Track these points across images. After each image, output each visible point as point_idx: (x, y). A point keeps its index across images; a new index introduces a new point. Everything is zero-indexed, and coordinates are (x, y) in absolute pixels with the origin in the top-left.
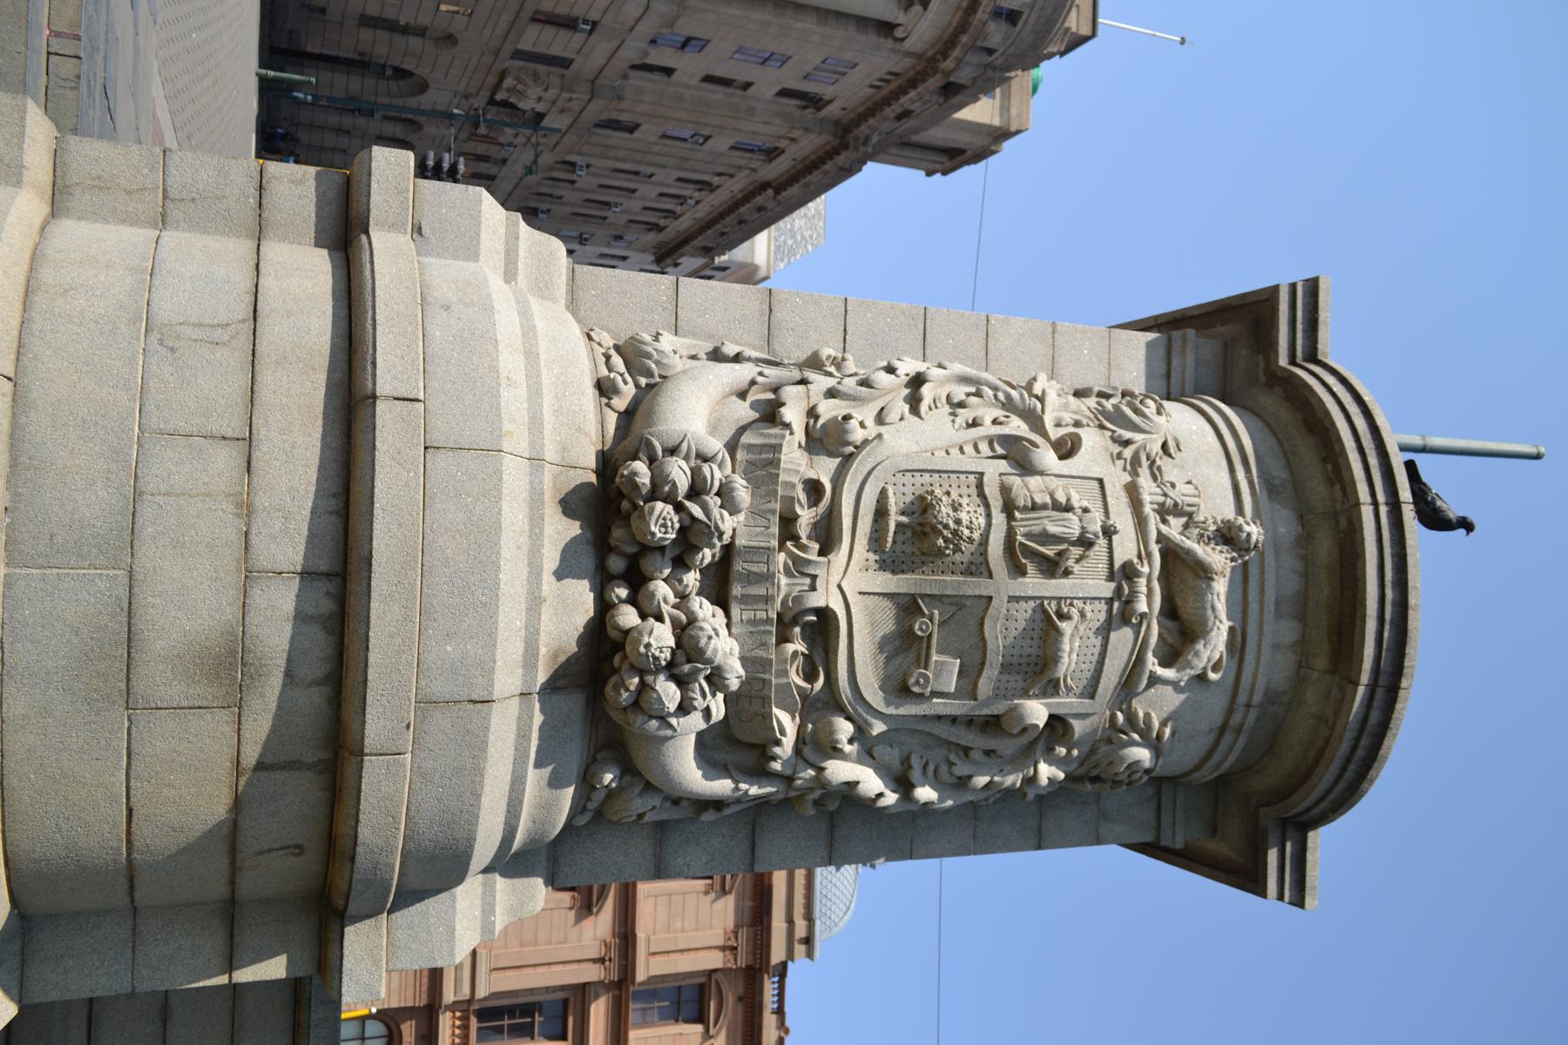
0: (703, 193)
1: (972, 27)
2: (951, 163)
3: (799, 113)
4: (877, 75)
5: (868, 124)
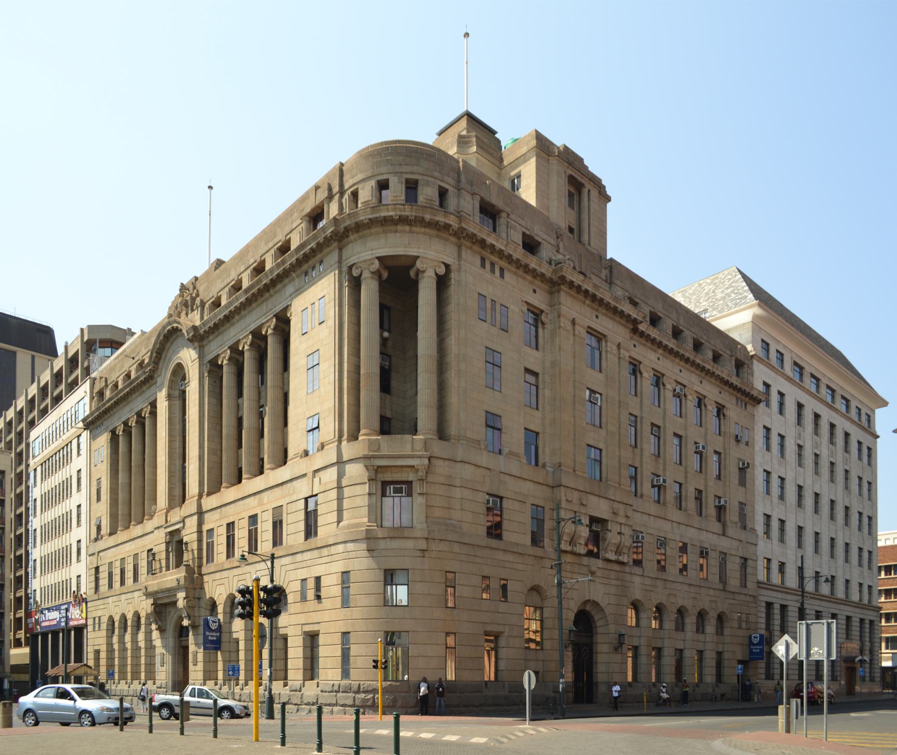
0: (666, 382)
1: (417, 215)
2: (586, 184)
3: (548, 326)
4: (488, 275)
5: (537, 268)
